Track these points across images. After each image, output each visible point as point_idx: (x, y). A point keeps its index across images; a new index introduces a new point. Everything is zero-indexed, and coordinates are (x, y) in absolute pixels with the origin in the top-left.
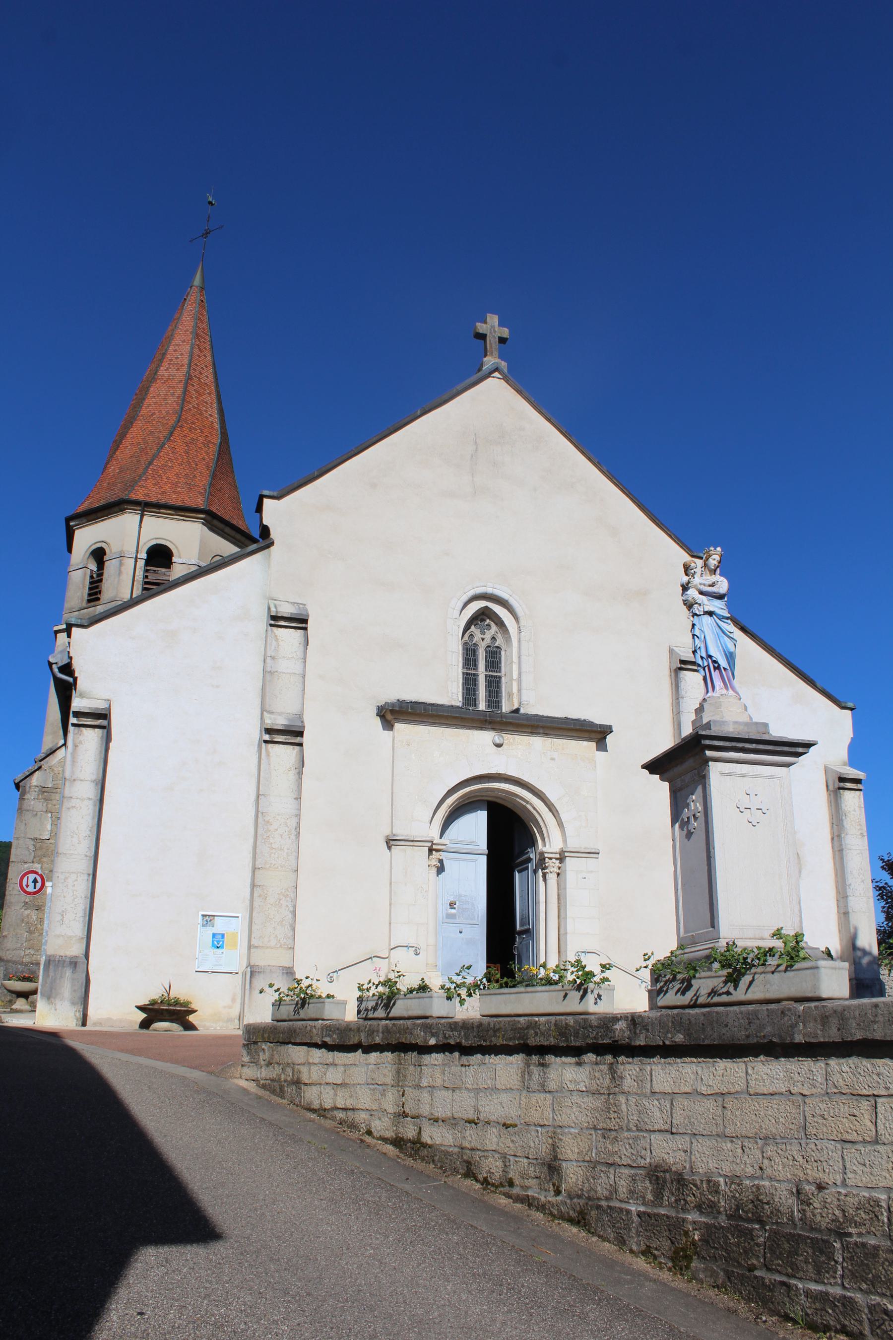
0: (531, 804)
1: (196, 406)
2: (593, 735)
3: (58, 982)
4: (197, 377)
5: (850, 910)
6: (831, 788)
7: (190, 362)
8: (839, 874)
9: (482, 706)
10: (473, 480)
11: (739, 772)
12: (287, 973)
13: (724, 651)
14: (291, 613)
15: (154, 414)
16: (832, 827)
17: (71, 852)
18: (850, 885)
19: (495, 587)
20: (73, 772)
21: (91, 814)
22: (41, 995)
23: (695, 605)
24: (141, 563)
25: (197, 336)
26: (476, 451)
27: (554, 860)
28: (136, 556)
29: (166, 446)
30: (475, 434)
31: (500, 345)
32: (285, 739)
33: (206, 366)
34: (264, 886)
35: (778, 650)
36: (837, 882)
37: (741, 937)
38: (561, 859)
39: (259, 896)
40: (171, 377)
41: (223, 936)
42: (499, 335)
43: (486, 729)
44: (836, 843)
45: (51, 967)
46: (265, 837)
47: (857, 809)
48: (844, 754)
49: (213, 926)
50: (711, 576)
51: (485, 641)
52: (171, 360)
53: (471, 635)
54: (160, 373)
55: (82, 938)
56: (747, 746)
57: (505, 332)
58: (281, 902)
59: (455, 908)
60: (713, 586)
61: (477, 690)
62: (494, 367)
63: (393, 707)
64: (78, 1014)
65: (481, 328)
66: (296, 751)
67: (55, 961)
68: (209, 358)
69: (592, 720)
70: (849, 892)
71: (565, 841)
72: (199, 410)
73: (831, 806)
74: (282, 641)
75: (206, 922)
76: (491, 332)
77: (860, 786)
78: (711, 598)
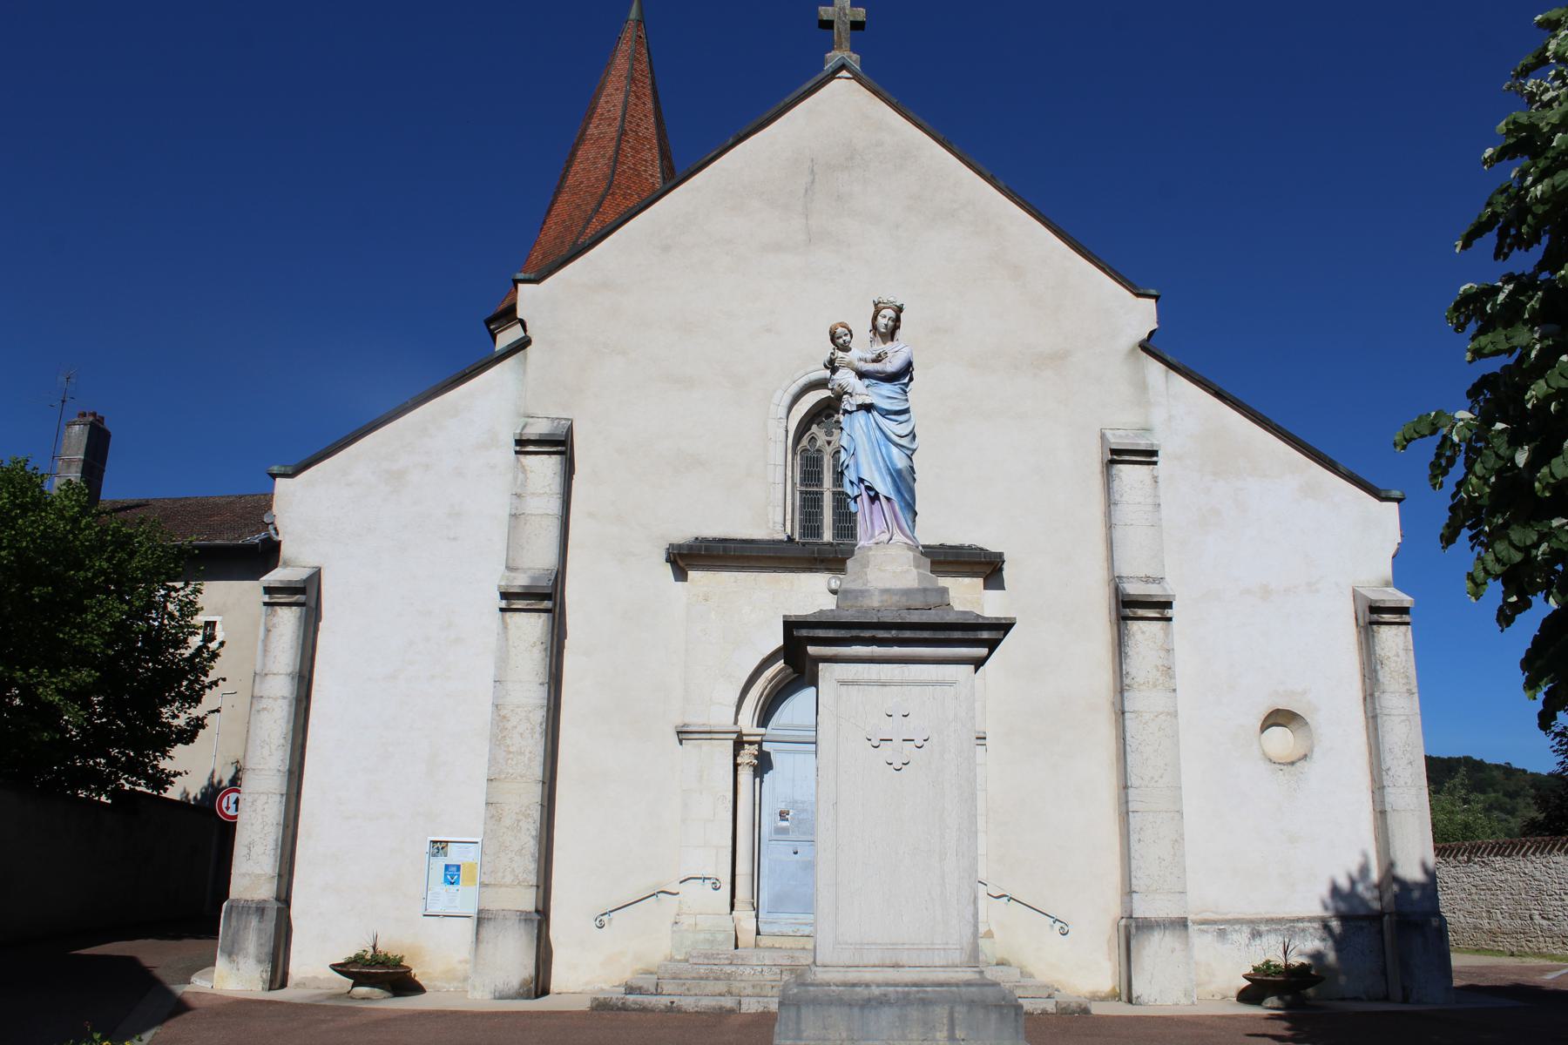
2: (976, 569)
3: (241, 933)
4: (633, 131)
5: (1388, 808)
6: (1361, 622)
7: (624, 115)
9: (828, 536)
10: (807, 223)
11: (874, 677)
12: (526, 920)
13: (889, 469)
14: (540, 434)
15: (582, 183)
16: (1364, 681)
17: (260, 767)
18: (1388, 769)
20: (264, 665)
21: (286, 718)
22: (221, 950)
23: (844, 396)
25: (633, 80)
29: (594, 220)
30: (812, 160)
31: (855, 32)
32: (528, 605)
33: (645, 116)
35: (1277, 420)
36: (1371, 764)
37: (856, 964)
41: (458, 867)
42: (852, 19)
43: (817, 570)
45: (233, 915)
47: (1402, 653)
48: (1386, 569)
49: (446, 856)
50: (885, 344)
52: (602, 114)
55: (273, 877)
56: (881, 634)
57: (860, 14)
58: (520, 824)
59: (787, 820)
60: (880, 361)
61: (822, 514)
62: (840, 63)
64: (264, 975)
65: (825, 12)
67: (238, 907)
68: (650, 105)
69: (981, 546)
70: (1387, 781)
73: (1362, 649)
74: (531, 472)
75: (436, 851)
76: (839, 18)
77: (1406, 618)
78: (875, 381)
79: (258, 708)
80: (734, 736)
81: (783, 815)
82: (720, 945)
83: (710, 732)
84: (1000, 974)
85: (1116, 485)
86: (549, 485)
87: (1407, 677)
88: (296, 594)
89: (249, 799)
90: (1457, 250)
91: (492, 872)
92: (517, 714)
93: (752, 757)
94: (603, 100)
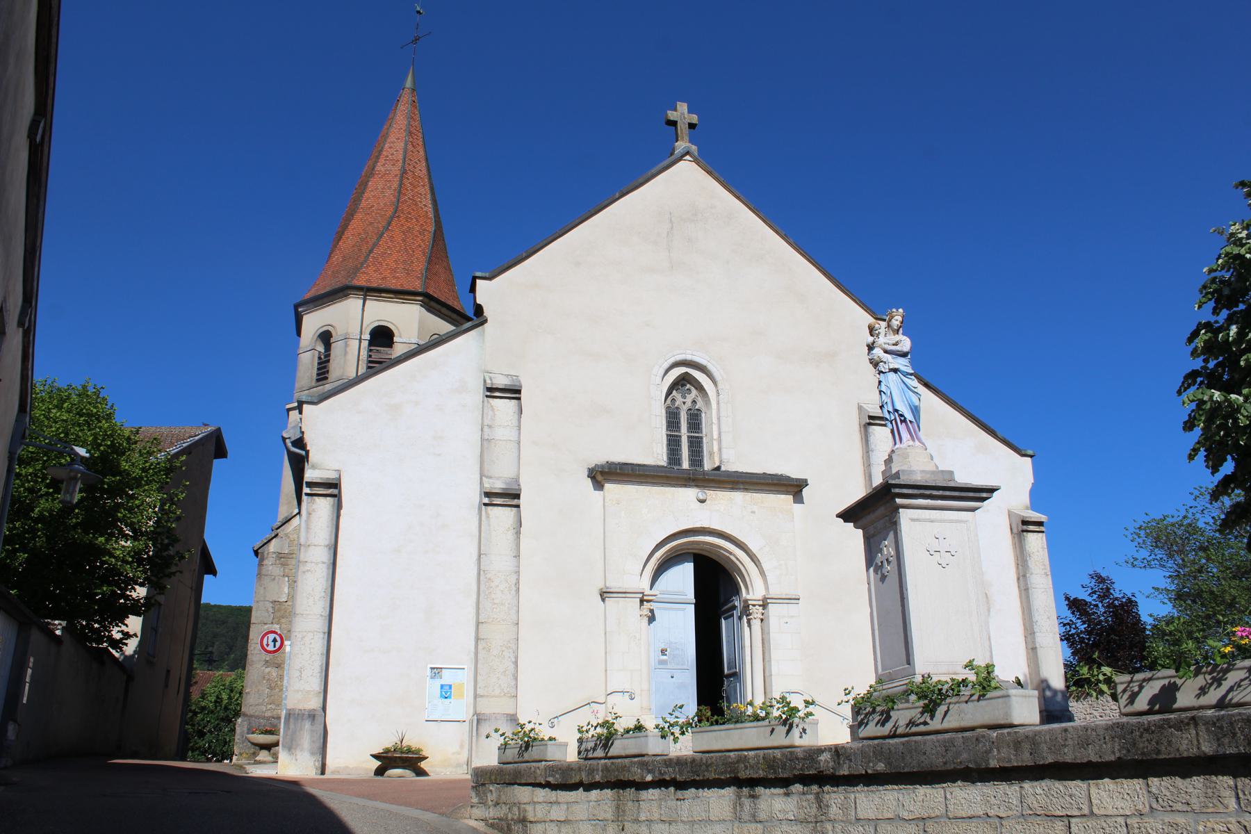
0: (734, 555)
2: (790, 489)
5: (1038, 646)
6: (1015, 531)
7: (405, 158)
9: (686, 465)
12: (511, 720)
16: (1018, 568)
17: (308, 613)
24: (365, 344)
25: (410, 133)
27: (757, 607)
28: (361, 337)
29: (385, 235)
30: (670, 214)
32: (504, 501)
33: (420, 161)
36: (1024, 619)
38: (764, 606)
41: (450, 686)
43: (690, 486)
47: (1040, 550)
48: (1026, 499)
49: (441, 678)
51: (686, 404)
52: (387, 156)
55: (320, 692)
56: (935, 493)
57: (694, 119)
61: (681, 450)
62: (685, 151)
65: (672, 115)
68: (422, 153)
71: (767, 588)
77: (1042, 529)
79: (304, 570)
80: (641, 595)
86: (510, 420)
87: (1044, 565)
88: (330, 488)
89: (299, 636)
90: (1196, 309)
91: (485, 687)
92: (498, 577)
94: (387, 146)
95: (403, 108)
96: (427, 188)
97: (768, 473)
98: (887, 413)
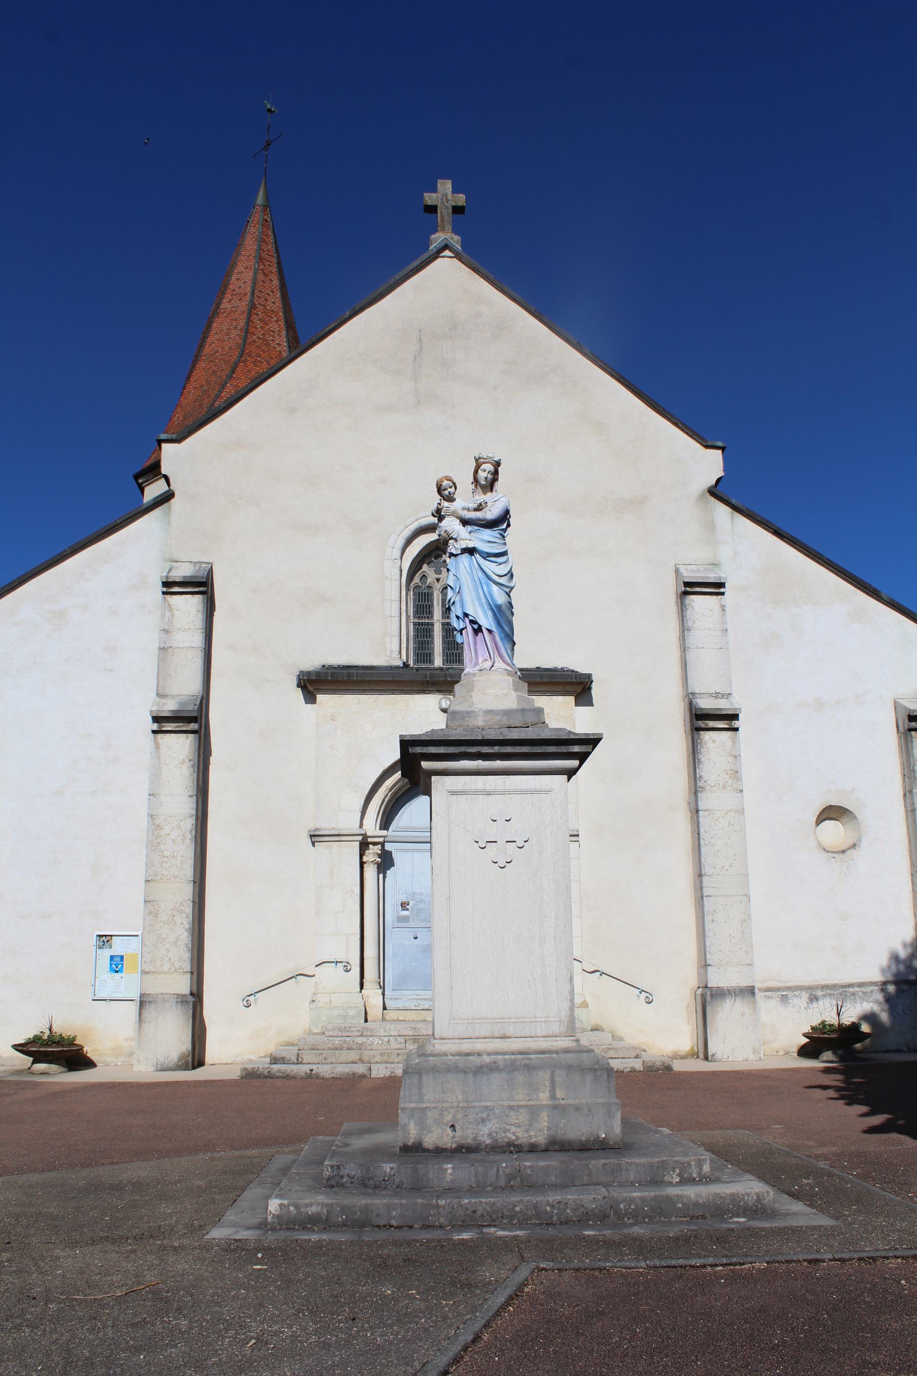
1: (261, 336)
2: (569, 688)
4: (262, 305)
8: (912, 841)
9: (438, 662)
12: (182, 1002)
13: (490, 605)
14: (184, 577)
15: (217, 351)
19: (419, 517)
23: (450, 541)
25: (261, 259)
26: (421, 350)
29: (229, 385)
30: (420, 330)
32: (176, 727)
33: (272, 291)
34: (154, 901)
37: (469, 1036)
39: (150, 913)
40: (234, 309)
41: (122, 957)
42: (453, 204)
44: (908, 800)
46: (155, 844)
49: (111, 948)
51: (440, 581)
52: (234, 290)
53: (424, 575)
54: (223, 306)
57: (461, 199)
59: (408, 910)
60: (481, 510)
61: (433, 642)
62: (443, 244)
63: (309, 677)
65: (430, 198)
66: (190, 739)
68: (276, 282)
69: (572, 668)
72: (265, 340)
74: (177, 610)
76: (442, 203)
78: (476, 528)
80: (360, 838)
81: (404, 906)
82: (352, 1019)
83: (339, 835)
84: (595, 1038)
85: (689, 613)
93: (376, 856)
94: (234, 278)
95: (253, 230)
96: (282, 323)
97: (544, 666)
98: (455, 619)
